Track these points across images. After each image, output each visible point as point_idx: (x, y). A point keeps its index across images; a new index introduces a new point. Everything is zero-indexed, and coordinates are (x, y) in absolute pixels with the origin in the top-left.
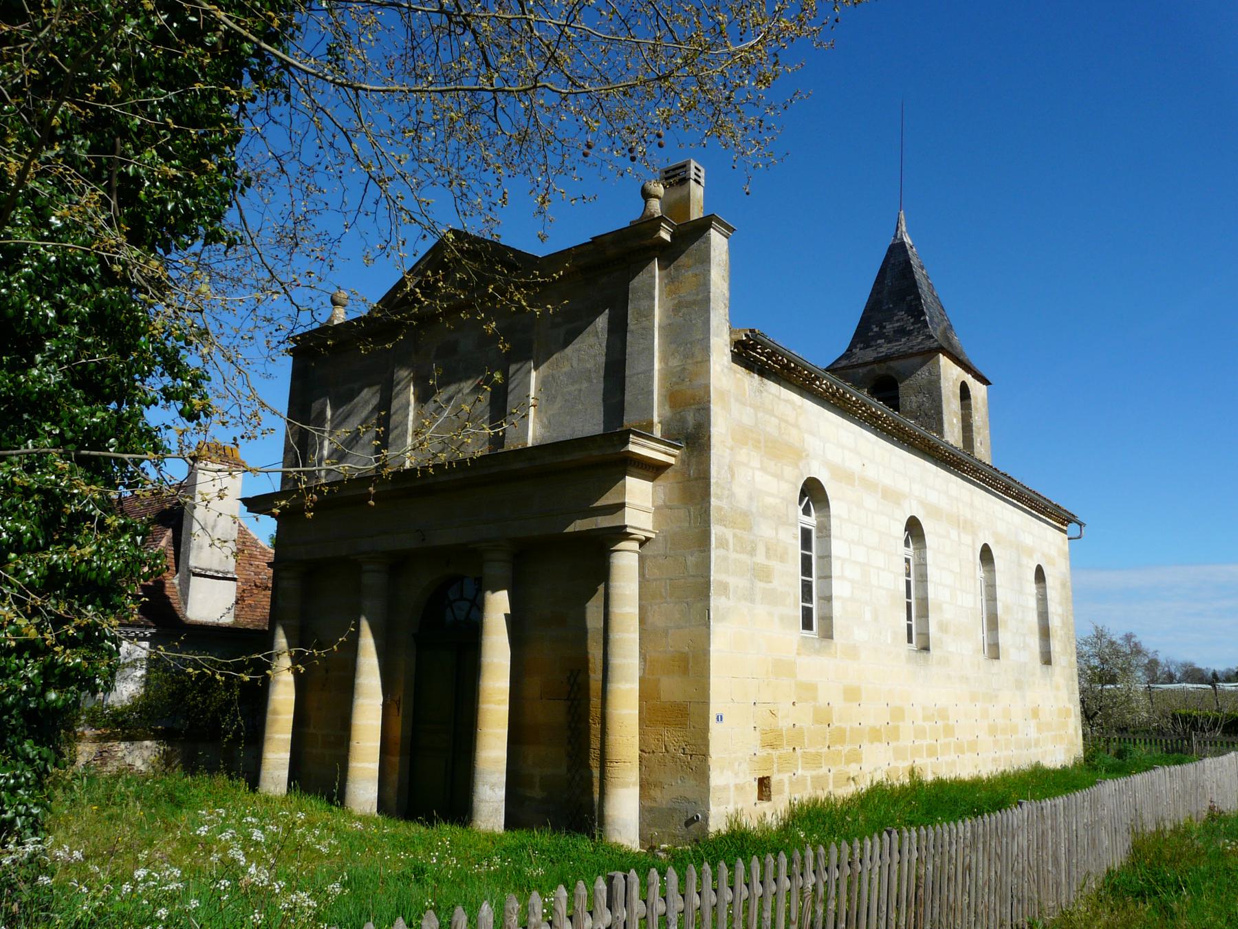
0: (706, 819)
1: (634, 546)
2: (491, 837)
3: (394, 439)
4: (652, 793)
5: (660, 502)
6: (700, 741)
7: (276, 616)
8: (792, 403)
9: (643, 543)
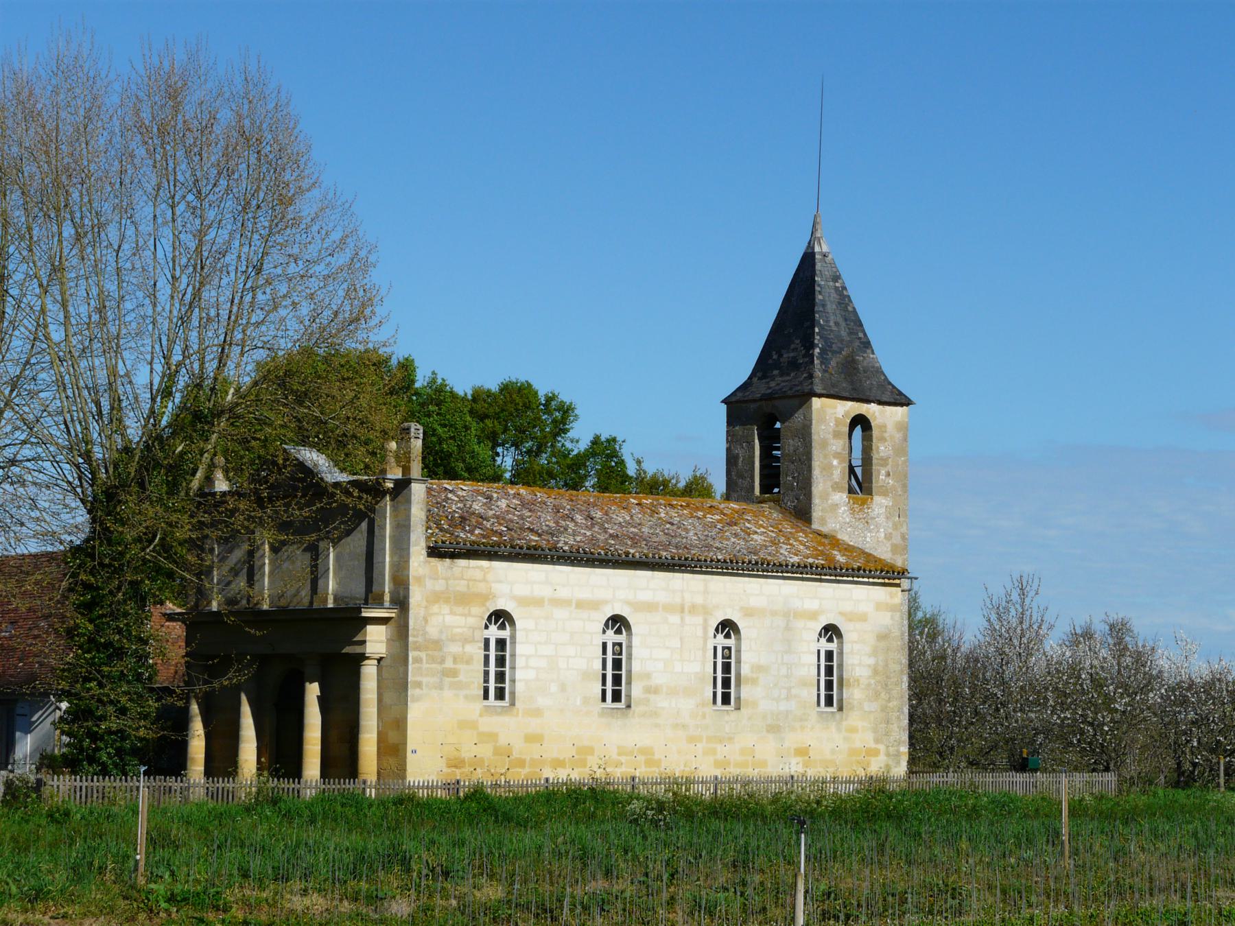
8: (481, 568)
9: (380, 660)
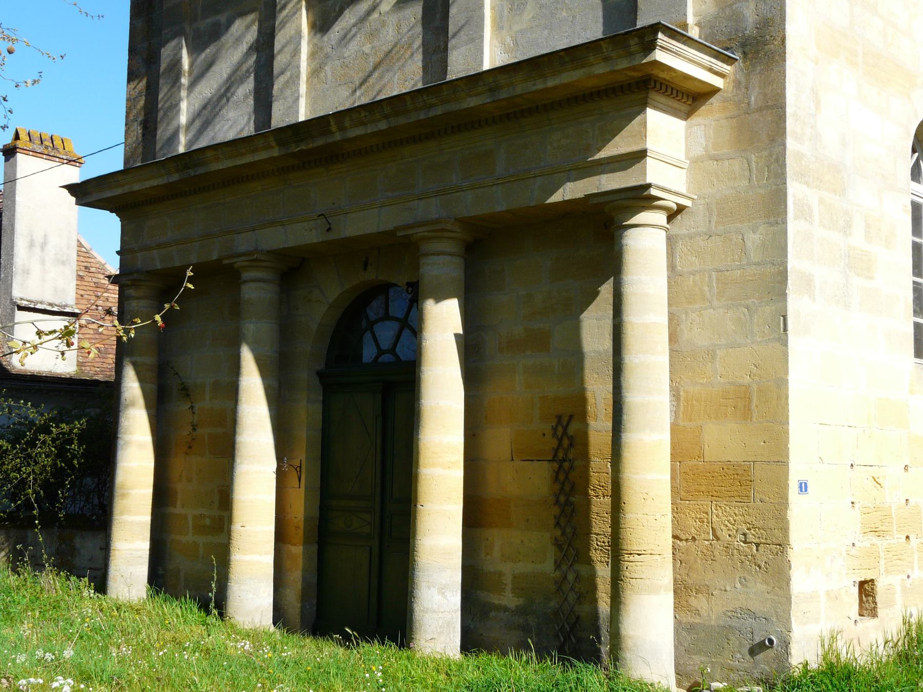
0: (786, 644)
1: (660, 218)
2: (444, 667)
3: (282, 90)
4: (693, 602)
5: (699, 151)
6: (772, 523)
7: (123, 351)
9: (673, 215)
